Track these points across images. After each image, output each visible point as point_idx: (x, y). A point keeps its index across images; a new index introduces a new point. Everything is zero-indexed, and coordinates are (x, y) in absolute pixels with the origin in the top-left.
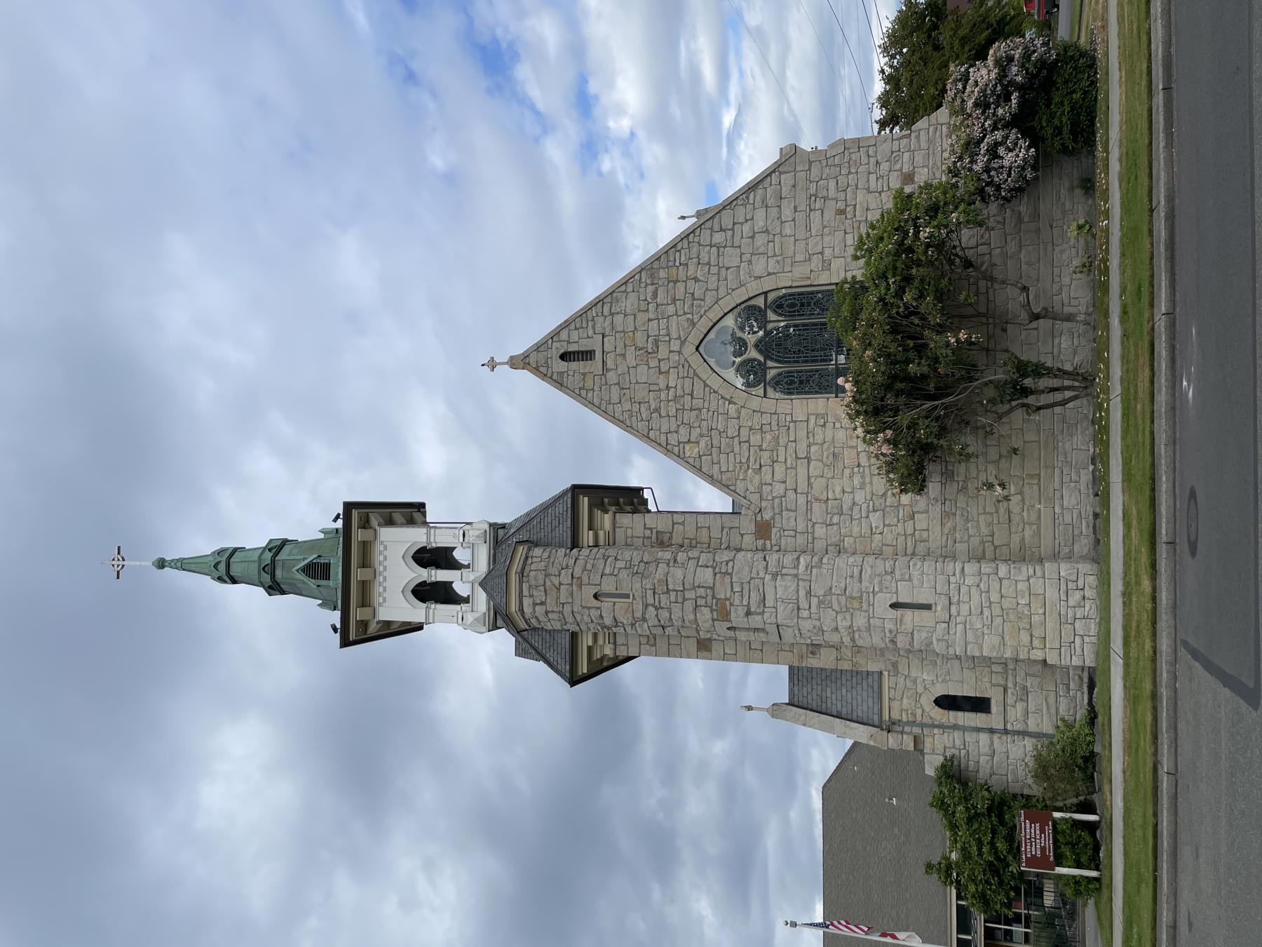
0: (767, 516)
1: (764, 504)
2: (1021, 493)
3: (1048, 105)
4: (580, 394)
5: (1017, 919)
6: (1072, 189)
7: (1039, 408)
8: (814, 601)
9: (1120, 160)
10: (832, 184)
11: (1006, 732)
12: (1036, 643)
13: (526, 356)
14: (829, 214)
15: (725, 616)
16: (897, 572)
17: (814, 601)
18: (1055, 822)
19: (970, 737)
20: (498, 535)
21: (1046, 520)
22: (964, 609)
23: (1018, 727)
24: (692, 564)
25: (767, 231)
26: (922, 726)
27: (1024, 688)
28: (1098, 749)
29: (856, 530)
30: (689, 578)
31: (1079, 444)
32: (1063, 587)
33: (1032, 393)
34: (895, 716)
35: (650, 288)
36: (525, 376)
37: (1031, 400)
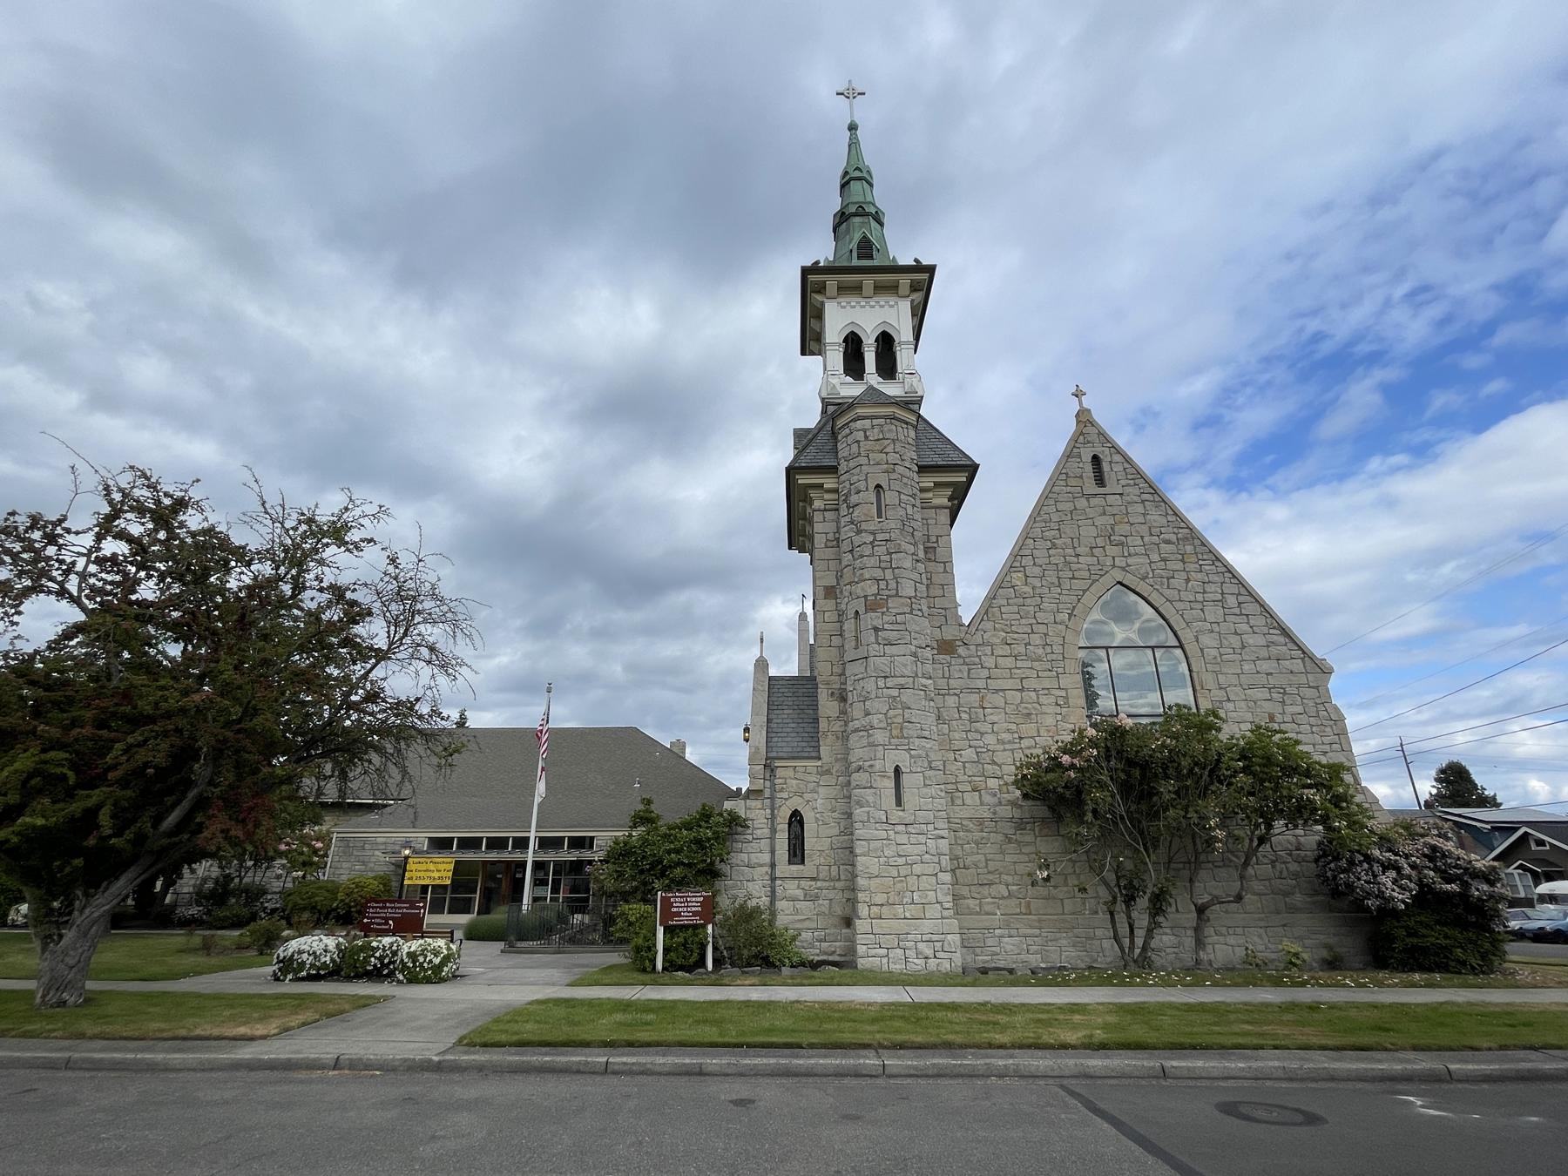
0: (961, 651)
1: (973, 648)
2: (1010, 895)
3: (1438, 922)
4: (1061, 474)
5: (555, 890)
6: (1329, 947)
7: (1112, 914)
8: (895, 693)
9: (1470, 1004)
10: (1299, 709)
11: (773, 879)
12: (875, 909)
13: (1092, 423)
14: (1268, 707)
15: (871, 608)
16: (932, 773)
17: (895, 693)
18: (704, 926)
19: (765, 844)
20: (911, 403)
21: (986, 921)
22: (903, 839)
23: (779, 891)
24: (916, 576)
25: (1244, 647)
26: (772, 798)
27: (817, 898)
28: (786, 971)
29: (957, 735)
30: (906, 574)
31: (1066, 953)
32: (935, 937)
33: (1128, 907)
34: (779, 772)
35: (1173, 538)
36: (1072, 426)
37: (1120, 906)
